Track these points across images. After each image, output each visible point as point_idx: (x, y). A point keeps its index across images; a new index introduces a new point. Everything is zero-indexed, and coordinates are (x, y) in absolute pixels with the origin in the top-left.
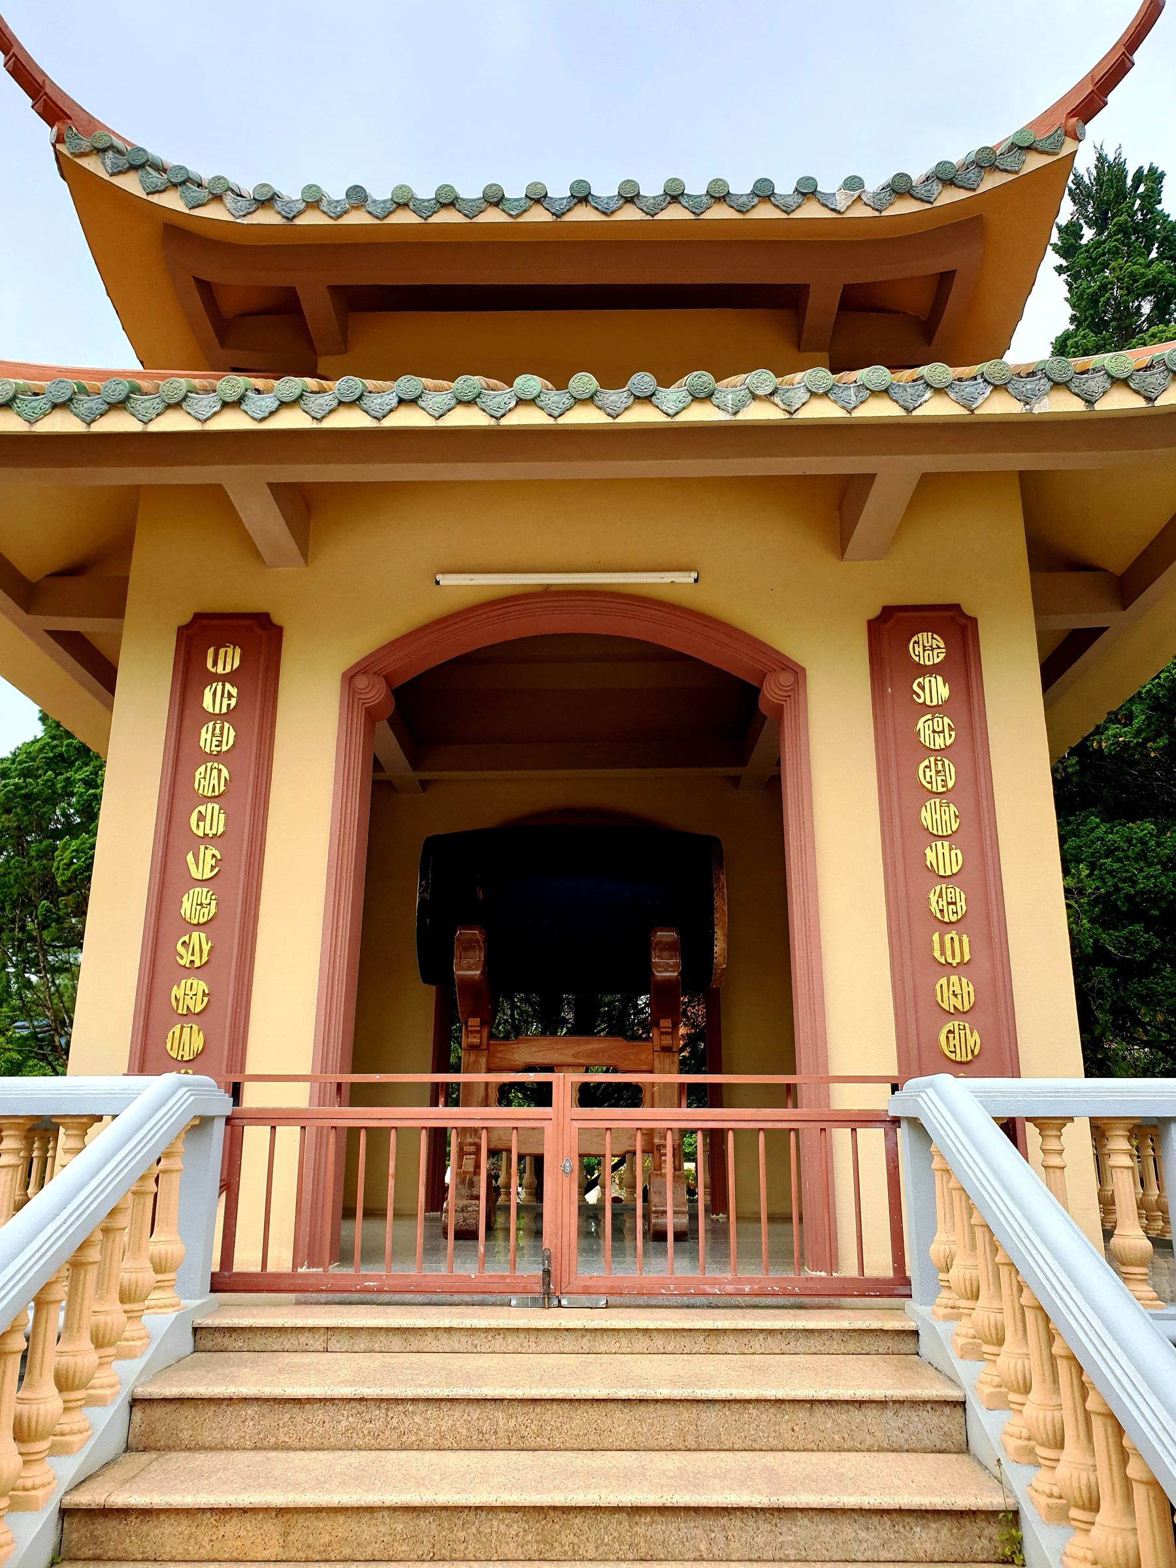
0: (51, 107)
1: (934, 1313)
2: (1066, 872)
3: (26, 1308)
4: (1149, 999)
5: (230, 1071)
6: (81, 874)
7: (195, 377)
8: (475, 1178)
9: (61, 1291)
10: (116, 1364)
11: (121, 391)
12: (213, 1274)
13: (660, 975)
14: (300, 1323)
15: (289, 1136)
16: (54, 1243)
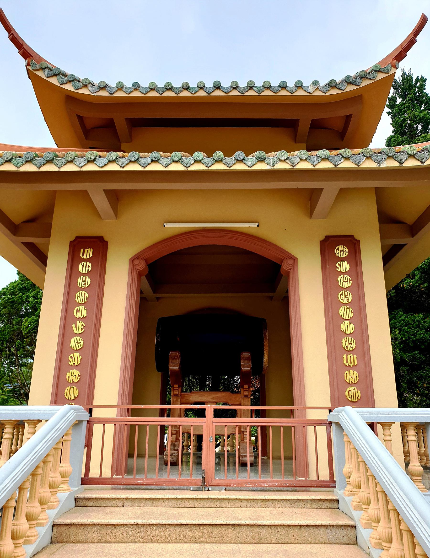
0: (26, 53)
1: (344, 493)
2: (391, 332)
3: (16, 490)
4: (420, 378)
5: (88, 404)
6: (32, 331)
7: (77, 151)
8: (176, 443)
9: (28, 485)
10: (48, 511)
11: (51, 156)
12: (82, 478)
13: (244, 369)
14: (114, 496)
15: (110, 428)
16: (26, 467)
